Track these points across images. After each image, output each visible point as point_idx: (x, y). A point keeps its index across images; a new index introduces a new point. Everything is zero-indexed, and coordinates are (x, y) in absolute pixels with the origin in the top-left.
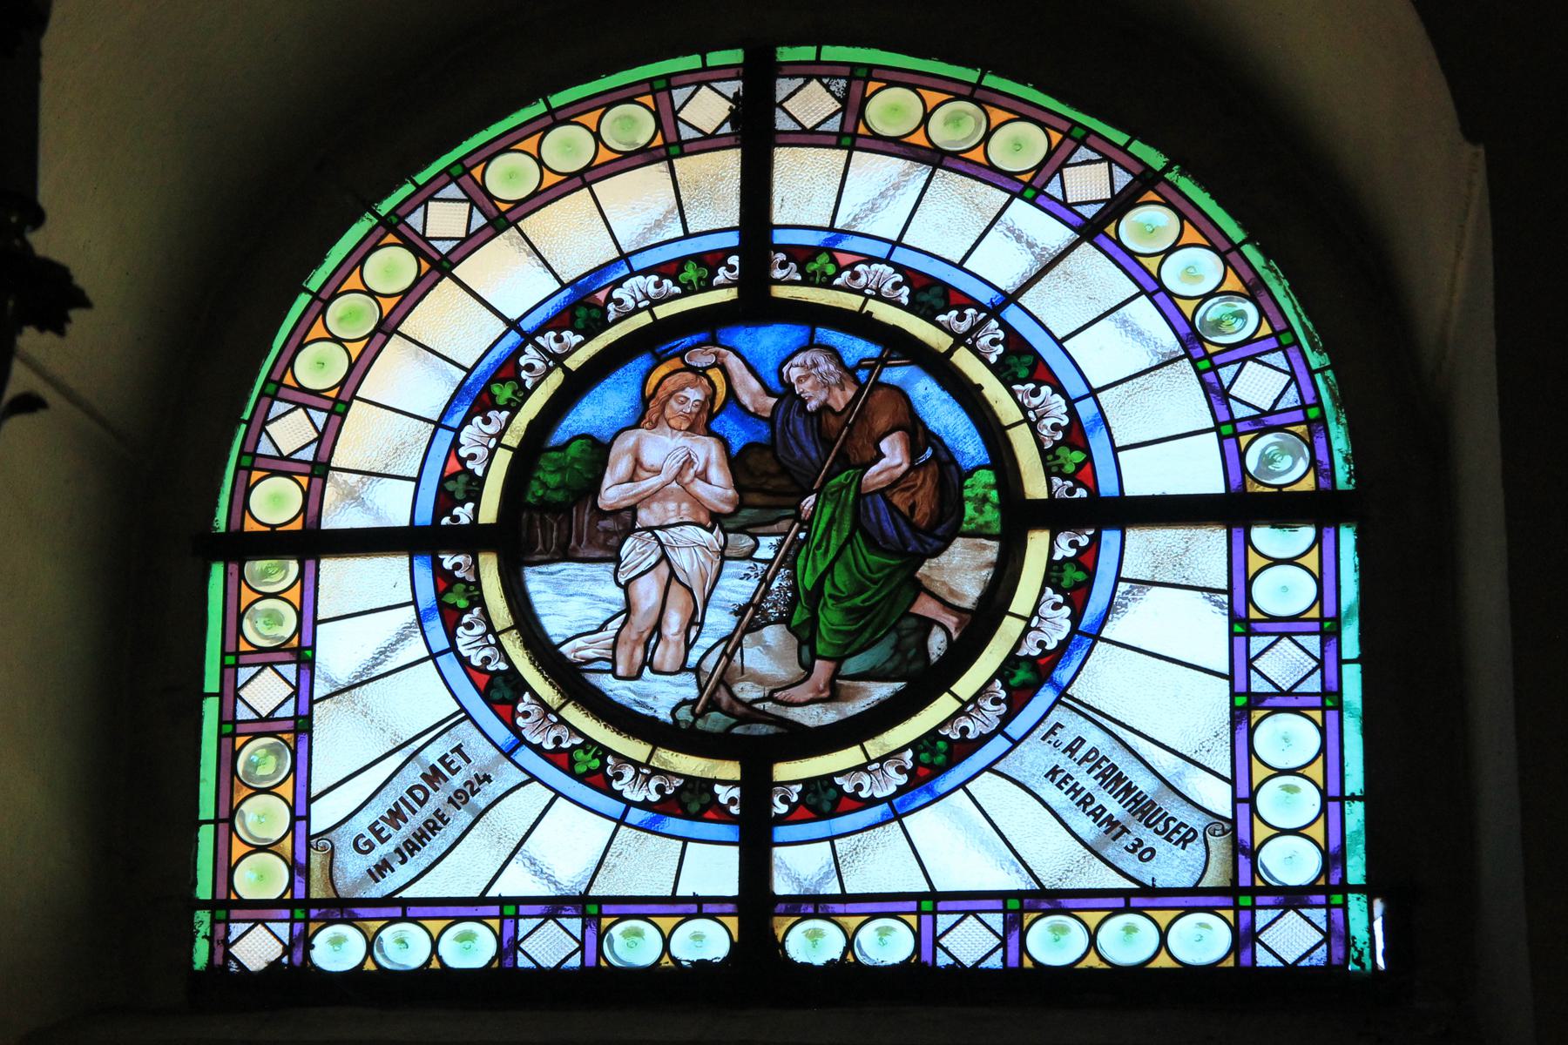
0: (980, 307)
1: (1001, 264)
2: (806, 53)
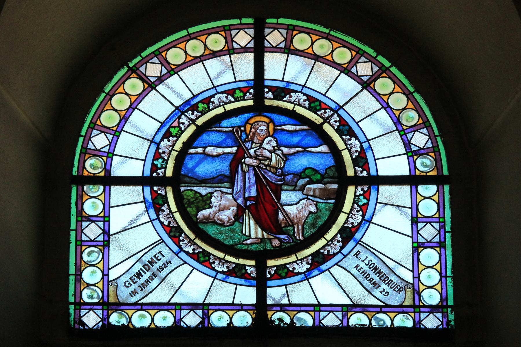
0: (331, 109)
1: (337, 96)
2: (274, 21)
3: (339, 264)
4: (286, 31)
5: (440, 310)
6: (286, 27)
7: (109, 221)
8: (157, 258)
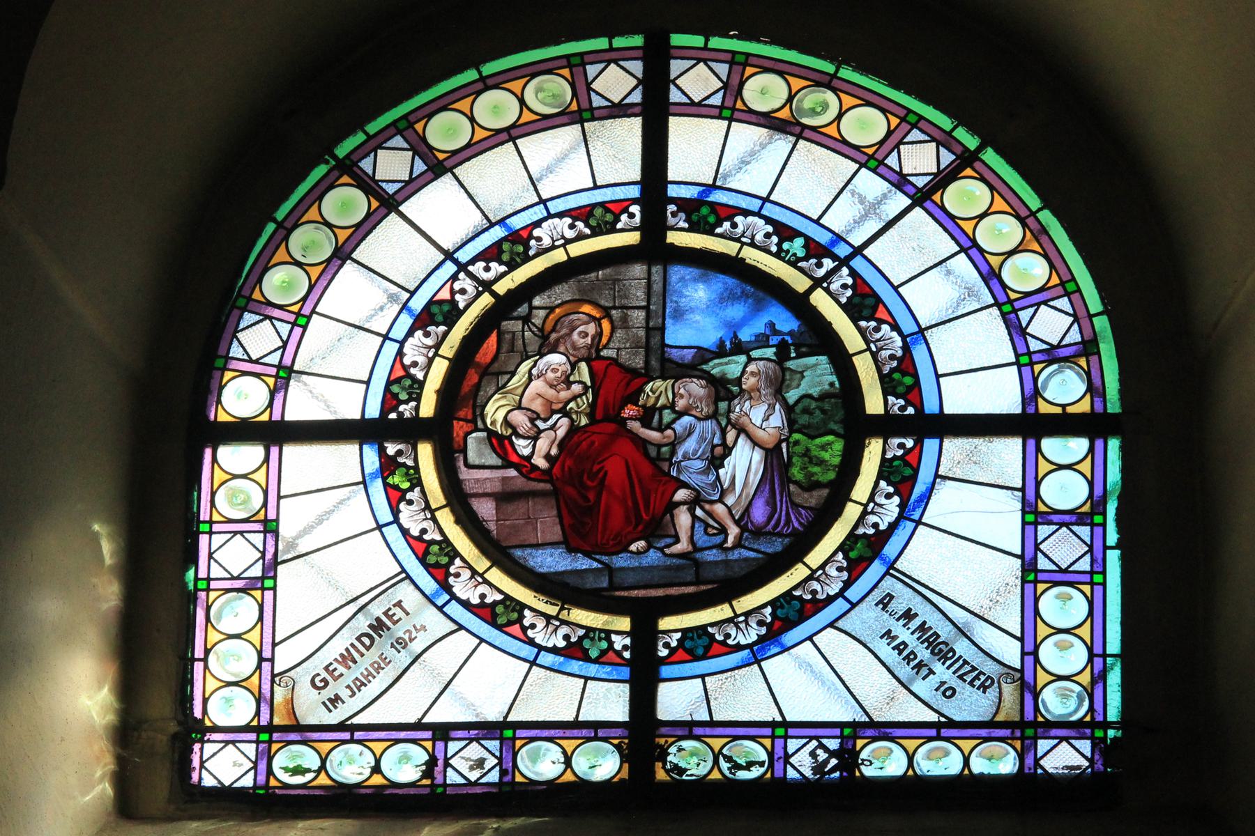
3: (840, 624)
4: (727, 66)
5: (1088, 731)
6: (729, 57)
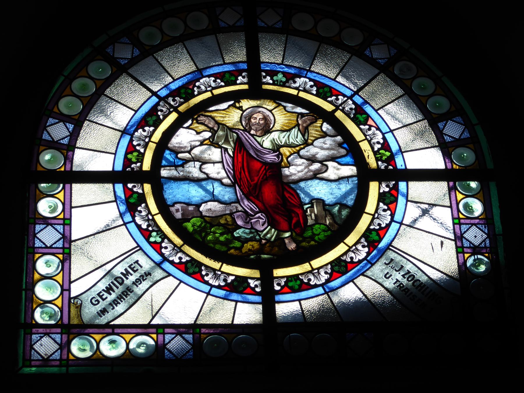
7: (70, 225)
8: (132, 269)
